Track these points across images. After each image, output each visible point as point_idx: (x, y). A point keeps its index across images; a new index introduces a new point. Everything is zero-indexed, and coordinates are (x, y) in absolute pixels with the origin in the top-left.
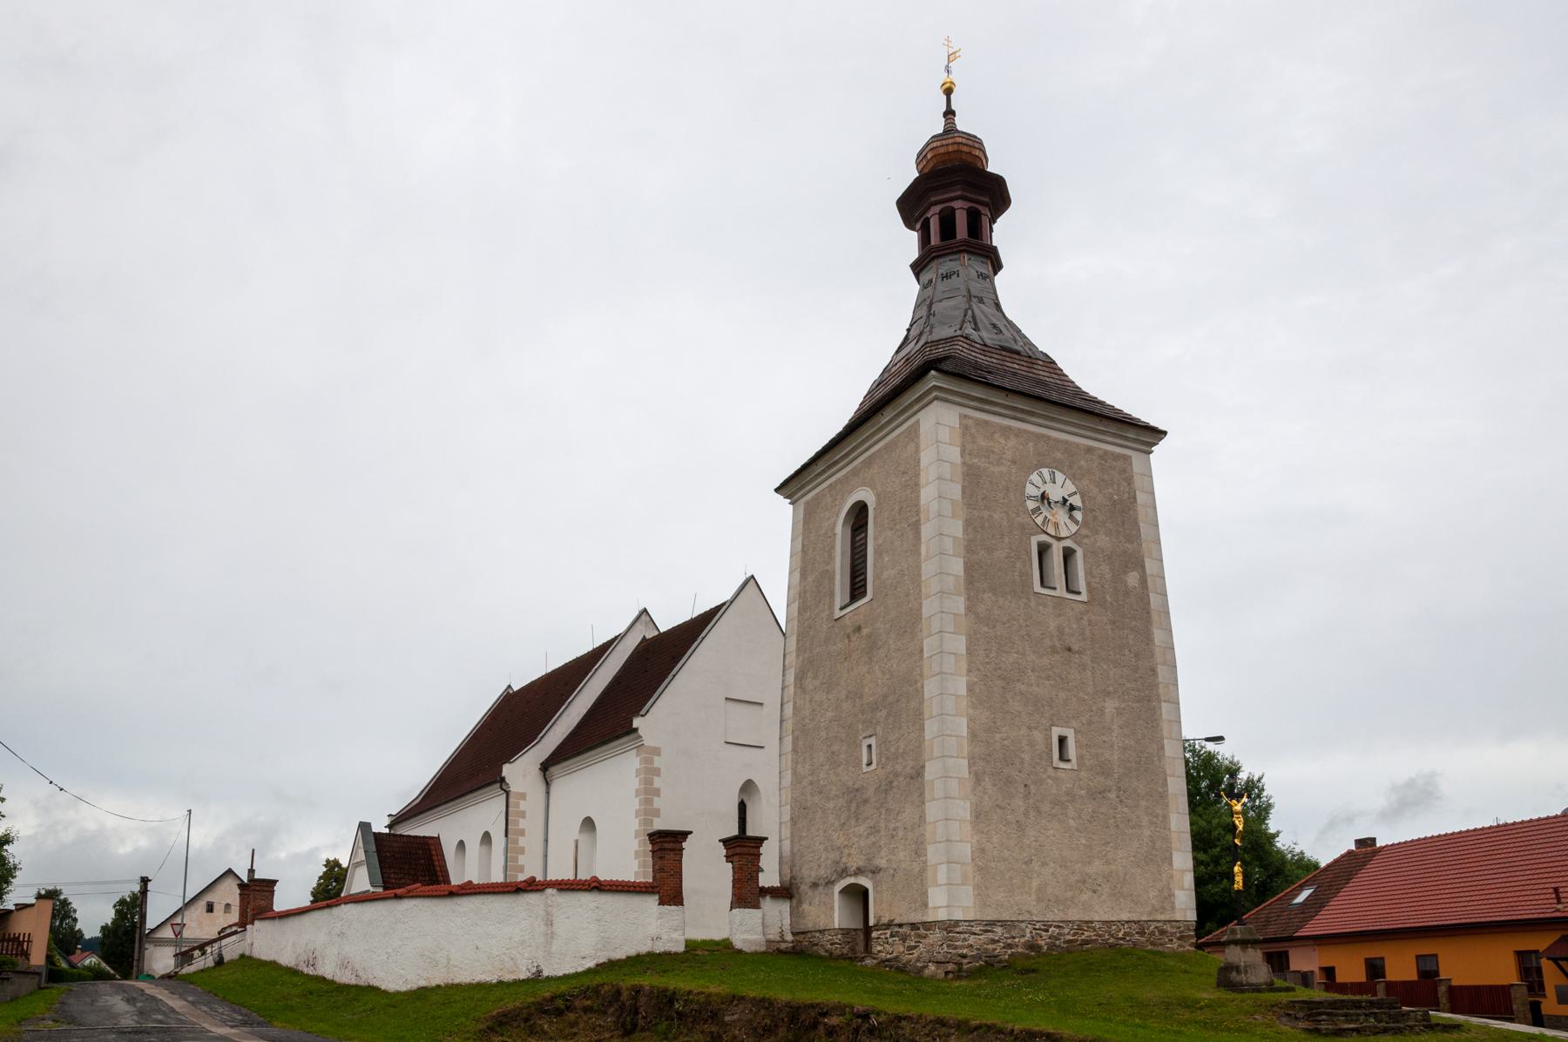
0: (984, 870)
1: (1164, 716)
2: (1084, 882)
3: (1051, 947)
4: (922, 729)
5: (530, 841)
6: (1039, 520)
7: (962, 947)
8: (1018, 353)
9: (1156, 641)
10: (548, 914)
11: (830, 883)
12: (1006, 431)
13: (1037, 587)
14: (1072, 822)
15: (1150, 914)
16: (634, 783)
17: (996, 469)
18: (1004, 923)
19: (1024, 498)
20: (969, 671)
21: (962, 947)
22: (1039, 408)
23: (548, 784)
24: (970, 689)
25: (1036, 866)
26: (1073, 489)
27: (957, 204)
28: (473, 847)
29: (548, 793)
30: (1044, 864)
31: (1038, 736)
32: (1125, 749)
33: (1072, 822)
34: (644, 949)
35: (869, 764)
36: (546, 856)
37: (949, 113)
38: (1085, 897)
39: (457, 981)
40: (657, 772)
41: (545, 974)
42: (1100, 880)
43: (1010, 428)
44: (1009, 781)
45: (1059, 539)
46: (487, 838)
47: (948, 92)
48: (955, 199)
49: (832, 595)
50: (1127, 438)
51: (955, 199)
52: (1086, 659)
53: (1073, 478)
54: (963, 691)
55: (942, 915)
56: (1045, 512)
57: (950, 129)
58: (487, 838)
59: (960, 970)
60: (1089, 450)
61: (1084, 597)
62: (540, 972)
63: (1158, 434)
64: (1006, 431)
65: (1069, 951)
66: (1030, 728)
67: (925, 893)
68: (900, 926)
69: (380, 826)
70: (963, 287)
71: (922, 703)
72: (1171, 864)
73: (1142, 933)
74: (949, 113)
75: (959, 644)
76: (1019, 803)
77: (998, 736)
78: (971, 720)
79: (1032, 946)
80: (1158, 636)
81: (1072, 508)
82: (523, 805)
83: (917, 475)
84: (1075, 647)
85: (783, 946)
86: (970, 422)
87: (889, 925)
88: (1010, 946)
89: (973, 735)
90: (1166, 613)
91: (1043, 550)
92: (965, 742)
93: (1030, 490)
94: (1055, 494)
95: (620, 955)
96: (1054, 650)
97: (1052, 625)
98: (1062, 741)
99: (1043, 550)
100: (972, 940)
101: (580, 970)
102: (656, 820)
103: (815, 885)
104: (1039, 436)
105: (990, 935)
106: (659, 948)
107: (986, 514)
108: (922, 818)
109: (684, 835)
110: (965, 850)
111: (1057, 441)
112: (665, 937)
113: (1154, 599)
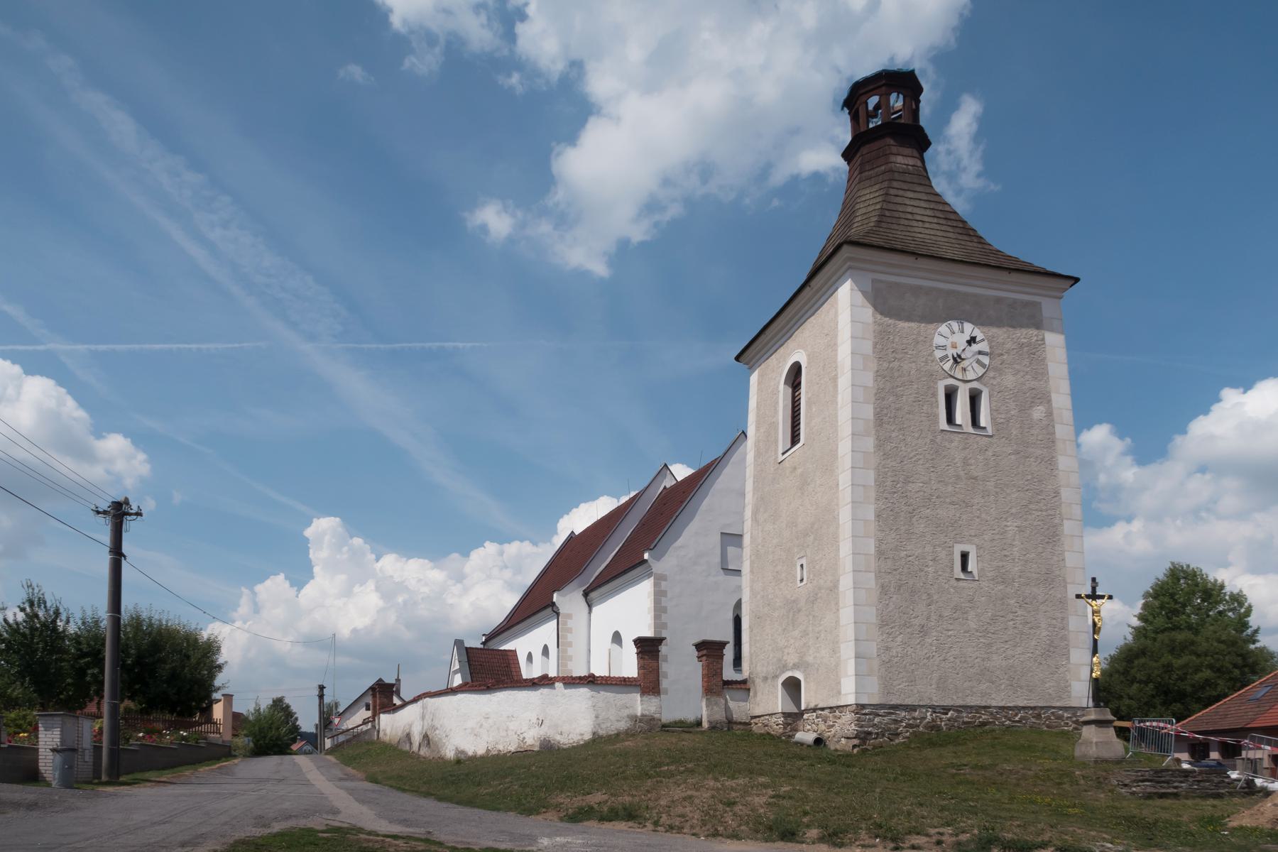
4: (838, 550)
5: (577, 651)
11: (776, 677)
28: (537, 656)
35: (802, 580)
36: (589, 662)
38: (983, 687)
43: (920, 287)
46: (546, 651)
49: (776, 441)
50: (809, 300)
54: (871, 516)
58: (546, 651)
60: (999, 300)
64: (916, 290)
67: (839, 683)
68: (823, 709)
69: (476, 643)
71: (837, 528)
72: (1068, 659)
78: (880, 541)
83: (836, 336)
87: (814, 710)
89: (880, 554)
98: (965, 556)
103: (765, 679)
105: (893, 717)
108: (837, 622)
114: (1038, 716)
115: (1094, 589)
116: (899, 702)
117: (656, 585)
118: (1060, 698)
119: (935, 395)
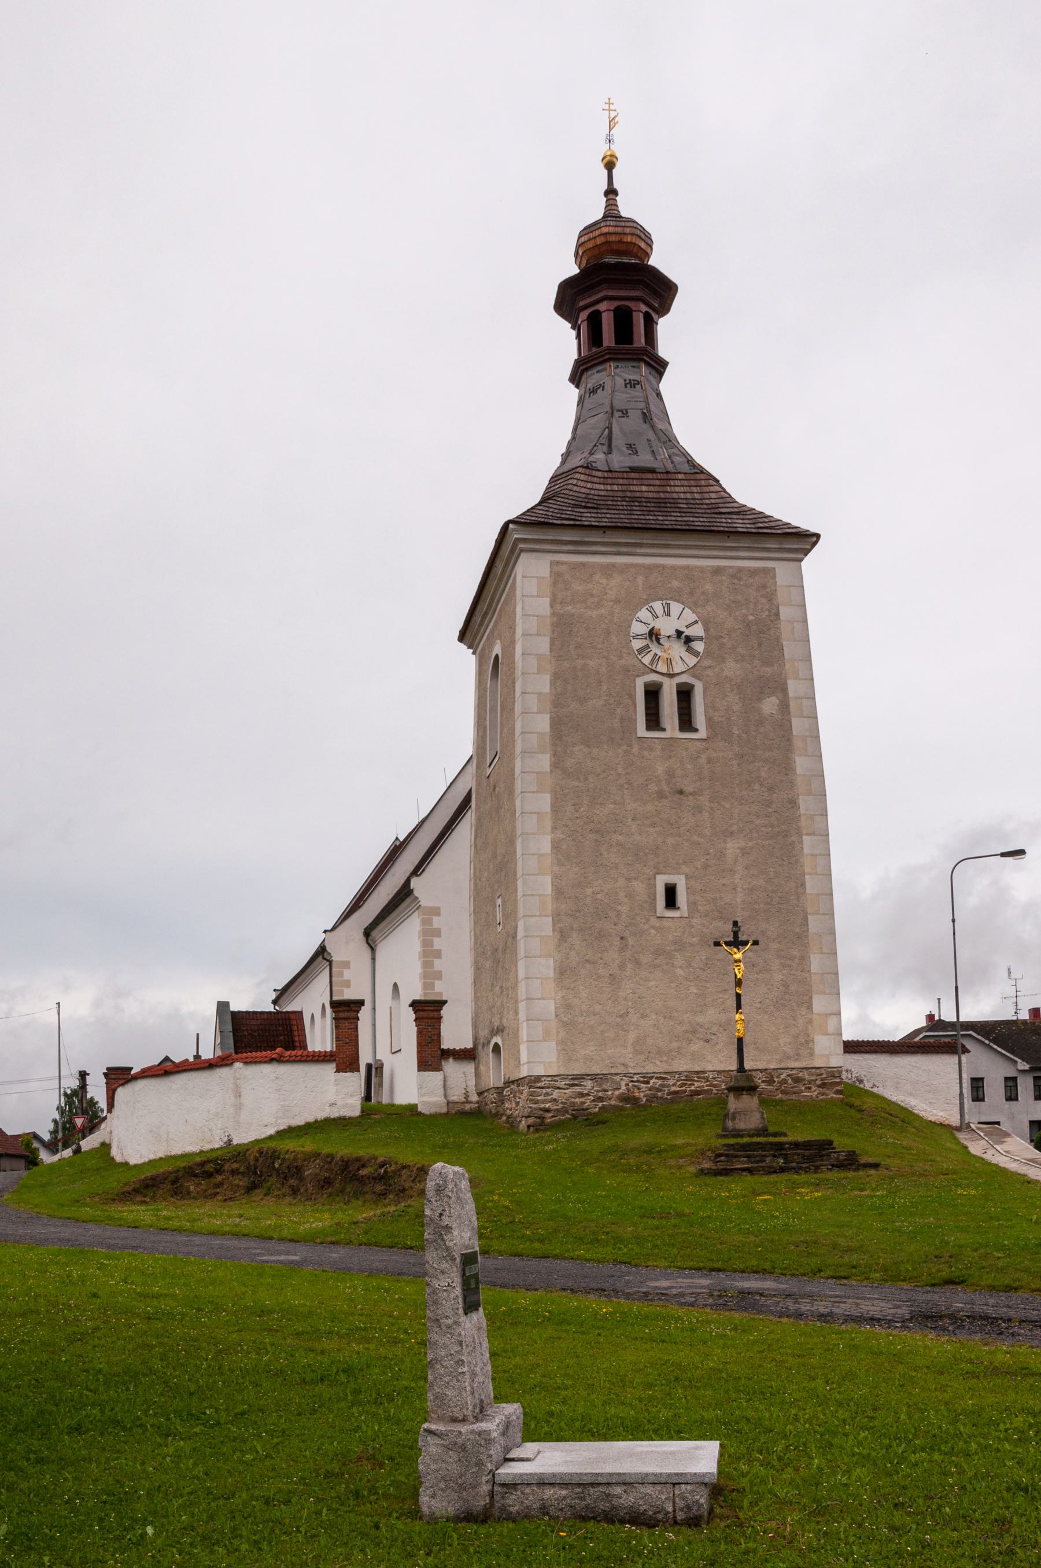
0: (570, 1027)
1: (807, 850)
2: (694, 1032)
3: (651, 1099)
6: (647, 660)
7: (544, 1102)
8: (652, 471)
9: (799, 771)
10: (237, 1086)
12: (608, 570)
13: (641, 730)
14: (679, 972)
15: (780, 1061)
16: (417, 946)
17: (594, 613)
18: (594, 1077)
19: (627, 637)
20: (554, 828)
21: (544, 1102)
22: (647, 538)
23: (373, 950)
24: (556, 846)
25: (633, 1017)
26: (693, 617)
27: (602, 307)
29: (373, 959)
30: (643, 1016)
31: (639, 886)
32: (751, 890)
33: (679, 972)
34: (321, 1115)
36: (374, 1025)
37: (611, 192)
38: (694, 1047)
39: (173, 1153)
40: (437, 933)
41: (235, 1142)
42: (714, 1029)
43: (613, 565)
44: (601, 935)
45: (671, 676)
47: (610, 166)
48: (615, 294)
51: (615, 294)
52: (704, 800)
53: (694, 607)
55: (524, 1072)
56: (655, 649)
57: (611, 213)
59: (542, 1123)
60: (718, 571)
61: (702, 733)
62: (230, 1141)
63: (800, 541)
64: (608, 570)
65: (672, 1101)
66: (629, 879)
70: (607, 402)
72: (810, 1007)
73: (770, 1082)
74: (611, 192)
75: (544, 802)
76: (613, 956)
77: (589, 891)
78: (556, 877)
79: (626, 1098)
80: (801, 764)
81: (688, 640)
82: (347, 974)
84: (689, 789)
85: (468, 1107)
86: (563, 568)
88: (601, 1099)
89: (559, 893)
90: (815, 736)
91: (653, 694)
92: (549, 900)
93: (637, 628)
94: (667, 627)
95: (299, 1121)
96: (661, 795)
97: (660, 769)
99: (653, 694)
100: (556, 1094)
101: (263, 1136)
102: (346, 990)
104: (650, 568)
105: (578, 1089)
106: (335, 1113)
107: (580, 662)
109: (445, 1002)
110: (549, 1007)
111: (674, 568)
112: (339, 1103)
113: (798, 726)
114: (770, 1082)
115: (736, 934)
116: (583, 1071)
117: (424, 922)
118: (798, 1056)
119: (632, 697)
